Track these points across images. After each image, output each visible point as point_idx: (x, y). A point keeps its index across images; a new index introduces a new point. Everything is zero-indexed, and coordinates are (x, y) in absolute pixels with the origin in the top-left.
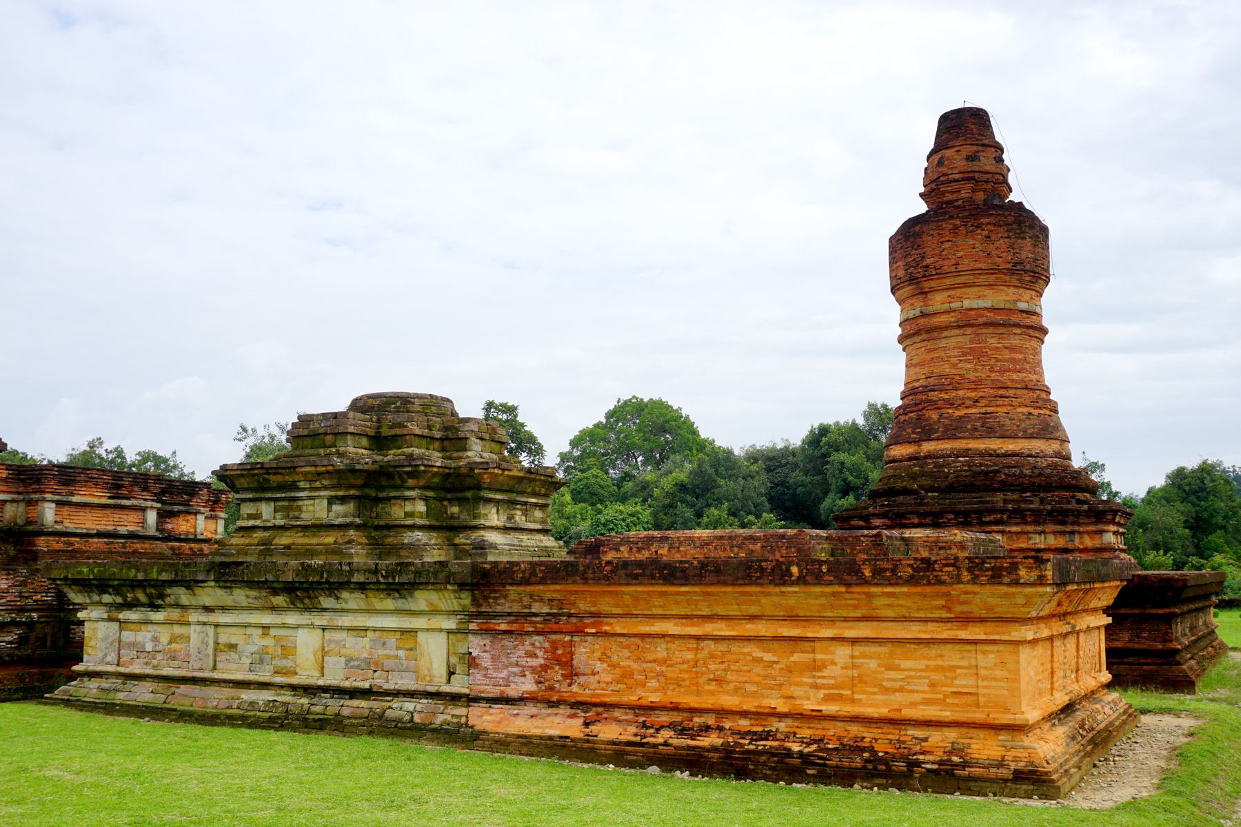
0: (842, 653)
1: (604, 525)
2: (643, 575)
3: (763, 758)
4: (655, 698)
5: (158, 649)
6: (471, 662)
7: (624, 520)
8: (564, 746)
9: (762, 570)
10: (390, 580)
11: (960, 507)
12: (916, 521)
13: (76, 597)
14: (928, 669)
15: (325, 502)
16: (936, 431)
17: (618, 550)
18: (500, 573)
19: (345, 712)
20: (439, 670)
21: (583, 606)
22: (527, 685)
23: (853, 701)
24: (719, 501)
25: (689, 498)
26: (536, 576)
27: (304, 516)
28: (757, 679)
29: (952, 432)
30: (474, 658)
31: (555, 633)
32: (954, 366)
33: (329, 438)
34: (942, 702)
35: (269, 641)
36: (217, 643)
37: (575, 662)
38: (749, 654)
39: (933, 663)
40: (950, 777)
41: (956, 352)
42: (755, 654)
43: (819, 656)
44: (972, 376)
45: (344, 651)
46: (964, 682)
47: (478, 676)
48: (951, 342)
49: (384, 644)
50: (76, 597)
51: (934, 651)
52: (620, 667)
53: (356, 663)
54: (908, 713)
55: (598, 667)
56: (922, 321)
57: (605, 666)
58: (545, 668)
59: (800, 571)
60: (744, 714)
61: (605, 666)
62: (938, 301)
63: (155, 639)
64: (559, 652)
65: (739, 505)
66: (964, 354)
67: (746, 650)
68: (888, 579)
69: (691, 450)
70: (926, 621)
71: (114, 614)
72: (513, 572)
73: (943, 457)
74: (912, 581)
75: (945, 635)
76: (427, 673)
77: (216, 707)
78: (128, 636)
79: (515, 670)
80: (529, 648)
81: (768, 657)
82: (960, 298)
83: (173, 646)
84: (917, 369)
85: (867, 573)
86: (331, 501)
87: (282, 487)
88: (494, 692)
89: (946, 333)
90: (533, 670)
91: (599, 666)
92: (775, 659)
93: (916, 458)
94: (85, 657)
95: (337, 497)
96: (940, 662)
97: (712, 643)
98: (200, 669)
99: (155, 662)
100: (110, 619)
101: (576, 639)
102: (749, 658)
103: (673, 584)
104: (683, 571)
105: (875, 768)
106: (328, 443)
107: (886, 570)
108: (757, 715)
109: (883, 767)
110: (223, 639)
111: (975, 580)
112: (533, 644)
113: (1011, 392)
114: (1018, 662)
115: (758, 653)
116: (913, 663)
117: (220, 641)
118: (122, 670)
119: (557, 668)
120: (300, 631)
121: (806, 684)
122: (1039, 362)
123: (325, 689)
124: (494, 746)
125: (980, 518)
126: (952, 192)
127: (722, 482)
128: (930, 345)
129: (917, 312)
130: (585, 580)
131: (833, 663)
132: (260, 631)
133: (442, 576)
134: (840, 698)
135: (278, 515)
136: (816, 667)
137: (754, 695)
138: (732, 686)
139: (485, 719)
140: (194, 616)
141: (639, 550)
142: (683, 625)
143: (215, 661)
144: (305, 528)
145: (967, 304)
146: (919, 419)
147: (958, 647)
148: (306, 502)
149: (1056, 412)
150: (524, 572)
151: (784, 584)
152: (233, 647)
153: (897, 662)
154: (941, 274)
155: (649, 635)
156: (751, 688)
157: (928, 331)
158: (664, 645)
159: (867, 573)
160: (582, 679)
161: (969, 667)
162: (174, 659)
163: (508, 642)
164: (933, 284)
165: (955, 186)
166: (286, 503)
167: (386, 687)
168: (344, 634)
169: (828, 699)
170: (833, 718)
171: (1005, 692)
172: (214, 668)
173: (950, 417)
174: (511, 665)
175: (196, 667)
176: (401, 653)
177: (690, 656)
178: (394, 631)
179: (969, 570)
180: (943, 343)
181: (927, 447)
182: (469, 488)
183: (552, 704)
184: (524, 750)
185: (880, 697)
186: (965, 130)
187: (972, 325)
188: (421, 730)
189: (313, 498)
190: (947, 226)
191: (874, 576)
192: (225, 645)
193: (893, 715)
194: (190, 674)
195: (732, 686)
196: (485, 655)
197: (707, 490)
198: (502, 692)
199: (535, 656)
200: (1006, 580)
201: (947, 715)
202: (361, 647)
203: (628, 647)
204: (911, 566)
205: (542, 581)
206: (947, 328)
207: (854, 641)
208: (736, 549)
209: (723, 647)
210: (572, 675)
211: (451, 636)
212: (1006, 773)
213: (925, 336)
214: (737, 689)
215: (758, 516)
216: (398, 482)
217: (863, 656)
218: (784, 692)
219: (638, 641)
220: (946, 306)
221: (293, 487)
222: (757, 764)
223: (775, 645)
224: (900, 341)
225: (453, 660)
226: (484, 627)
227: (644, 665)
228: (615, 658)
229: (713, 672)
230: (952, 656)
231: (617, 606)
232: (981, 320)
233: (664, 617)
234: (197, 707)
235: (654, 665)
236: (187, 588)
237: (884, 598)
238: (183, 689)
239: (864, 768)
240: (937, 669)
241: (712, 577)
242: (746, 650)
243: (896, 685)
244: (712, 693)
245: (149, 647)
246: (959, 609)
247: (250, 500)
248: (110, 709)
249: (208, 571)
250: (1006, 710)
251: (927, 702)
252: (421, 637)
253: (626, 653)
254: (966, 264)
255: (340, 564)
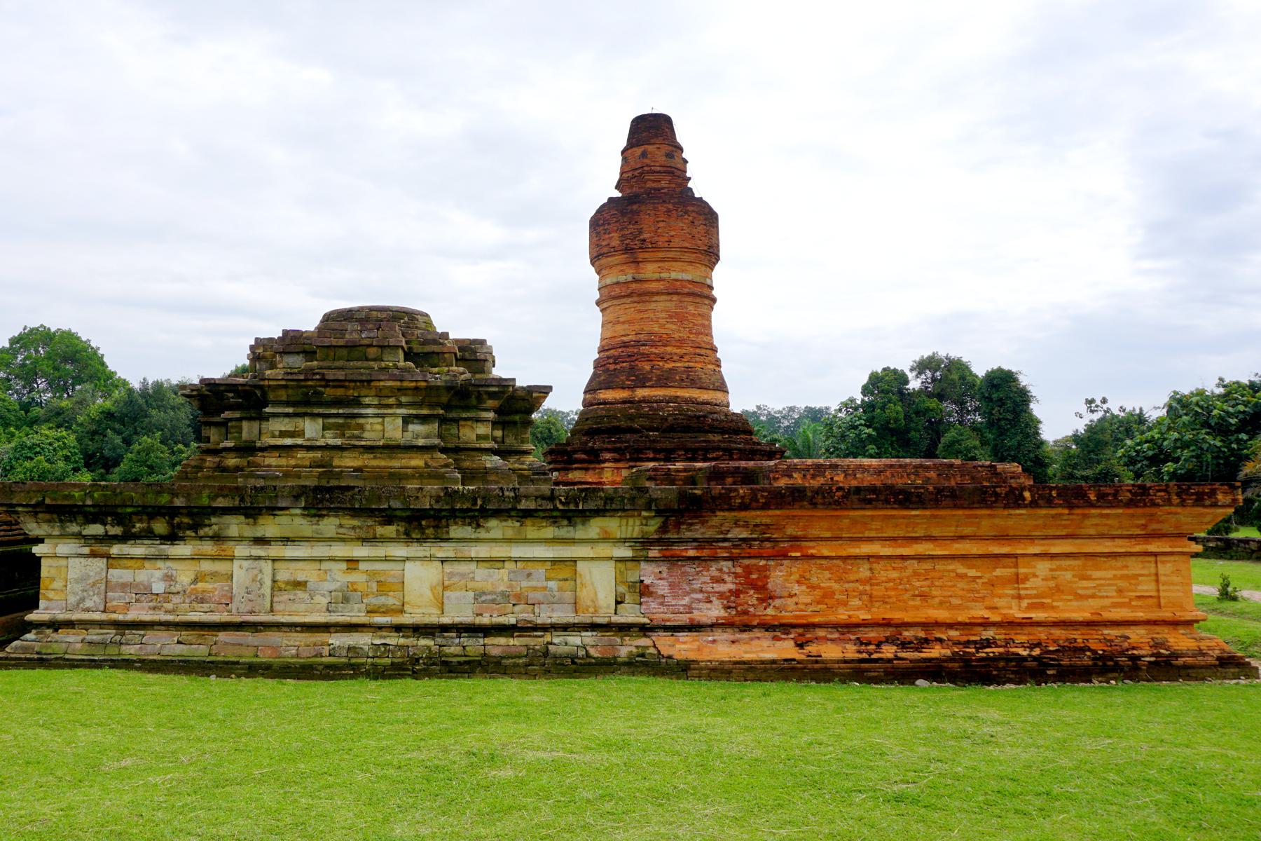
0: (1043, 567)
1: (30, 448)
2: (877, 500)
3: (1002, 664)
4: (863, 615)
5: (173, 589)
6: (644, 591)
7: (50, 444)
8: (793, 668)
9: (997, 495)
10: (572, 507)
11: (689, 445)
12: (651, 456)
13: (33, 528)
14: (1115, 577)
15: (400, 421)
16: (650, 380)
17: (790, 476)
18: (714, 498)
19: (495, 652)
20: (605, 599)
21: (791, 531)
22: (715, 611)
23: (1053, 608)
24: (149, 431)
25: (117, 426)
26: (757, 501)
27: (366, 435)
28: (961, 593)
29: (664, 380)
30: (648, 586)
31: (750, 557)
32: (662, 326)
33: (372, 352)
34: (1127, 605)
35: (355, 577)
36: (274, 581)
37: (769, 586)
38: (953, 571)
39: (1119, 573)
40: (1166, 668)
41: (663, 315)
42: (959, 571)
43: (1022, 571)
44: (676, 335)
45: (471, 585)
46: (1145, 588)
47: (653, 605)
48: (660, 306)
49: (529, 575)
50: (33, 528)
51: (1119, 562)
52: (820, 588)
53: (489, 597)
54: (1107, 615)
55: (793, 589)
56: (634, 285)
57: (804, 588)
58: (737, 593)
59: (1032, 496)
60: (950, 626)
61: (804, 588)
62: (649, 270)
63: (169, 578)
64: (754, 576)
65: (168, 434)
66: (671, 317)
67: (951, 567)
68: (1110, 502)
69: (99, 379)
70: (1113, 537)
71: (102, 549)
72: (731, 498)
73: (656, 402)
74: (1130, 504)
75: (1137, 549)
76: (589, 603)
77: (297, 656)
78: (118, 575)
79: (700, 596)
80: (716, 574)
81: (972, 573)
82: (668, 270)
83: (200, 585)
84: (626, 326)
85: (1093, 497)
86: (407, 420)
87: (338, 402)
88: (684, 619)
89: (656, 298)
90: (721, 595)
91: (796, 589)
92: (979, 574)
93: (630, 402)
94: (42, 603)
95: (417, 417)
96: (1125, 572)
97: (915, 562)
98: (251, 612)
99: (169, 606)
100: (94, 555)
101: (772, 563)
102: (953, 574)
103: (908, 508)
104: (919, 496)
105: (1104, 664)
106: (370, 357)
107: (1108, 494)
108: (925, 625)
109: (1111, 663)
110: (284, 575)
111: (1183, 504)
112: (720, 570)
113: (703, 352)
114: (1189, 570)
115: (961, 569)
116: (1103, 573)
117: (278, 578)
118: (114, 616)
119: (752, 592)
120: (408, 565)
121: (1007, 595)
122: (710, 327)
123: (444, 628)
124: (713, 674)
125: (705, 455)
126: (654, 181)
127: (154, 412)
128: (639, 306)
129: (630, 278)
130: (814, 505)
131: (1035, 576)
132: (344, 566)
133: (641, 502)
134: (1042, 606)
135: (328, 434)
136: (1017, 579)
137: (958, 607)
138: (937, 600)
139: (682, 647)
140: (241, 550)
141: (813, 477)
142: (890, 546)
143: (272, 602)
144: (370, 449)
145: (674, 275)
146: (632, 368)
147: (1141, 558)
148: (370, 420)
149: (719, 366)
150: (742, 498)
151: (1019, 507)
152: (299, 585)
153: (1089, 573)
154: (656, 248)
155: (856, 557)
156: (955, 601)
157: (640, 295)
158: (867, 566)
159: (1093, 497)
160: (777, 602)
161: (1149, 575)
162: (202, 601)
163: (689, 569)
164: (646, 255)
165: (657, 176)
166: (341, 421)
167: (539, 621)
168: (473, 566)
169: (1032, 607)
170: (1039, 624)
171: (1180, 594)
172: (272, 611)
173: (661, 369)
174: (694, 591)
175: (244, 608)
176: (552, 584)
177: (895, 575)
178: (543, 561)
179: (1178, 495)
180: (652, 306)
181: (641, 393)
182: (517, 412)
183: (746, 628)
184: (750, 676)
185: (1075, 603)
186: (651, 132)
187: (678, 294)
188: (611, 664)
189: (383, 416)
190: (662, 208)
191: (1098, 500)
192: (288, 583)
193: (1095, 618)
194: (238, 619)
195: (937, 600)
196: (661, 582)
197: (135, 419)
198: (691, 620)
199: (723, 581)
200: (1208, 503)
201: (1141, 615)
202: (498, 579)
203: (828, 569)
204: (1130, 491)
205: (765, 507)
206: (658, 294)
207: (1053, 556)
208: (913, 477)
209: (927, 565)
210: (767, 597)
211: (619, 565)
212: (1086, 660)
213: (636, 299)
214: (941, 603)
215: (187, 445)
216: (474, 401)
217: (1059, 568)
218: (987, 603)
219: (839, 562)
220: (657, 276)
221: (357, 402)
222: (997, 668)
223: (979, 562)
224: (598, 303)
225: (622, 589)
226: (668, 553)
227: (847, 585)
228: (814, 580)
229: (917, 588)
230: (1135, 566)
231: (828, 529)
232: (686, 290)
233: (870, 540)
234: (264, 657)
235: (857, 585)
236: (247, 516)
237: (1096, 519)
238: (223, 636)
239: (1095, 665)
240: (1122, 577)
241: (948, 502)
242: (951, 567)
243: (1089, 592)
244: (917, 608)
245: (158, 587)
246: (1154, 526)
247: (287, 415)
248: (43, 662)
249: (296, 497)
250: (1182, 608)
251: (1115, 605)
252: (581, 566)
253: (827, 574)
254: (676, 242)
255: (502, 489)
